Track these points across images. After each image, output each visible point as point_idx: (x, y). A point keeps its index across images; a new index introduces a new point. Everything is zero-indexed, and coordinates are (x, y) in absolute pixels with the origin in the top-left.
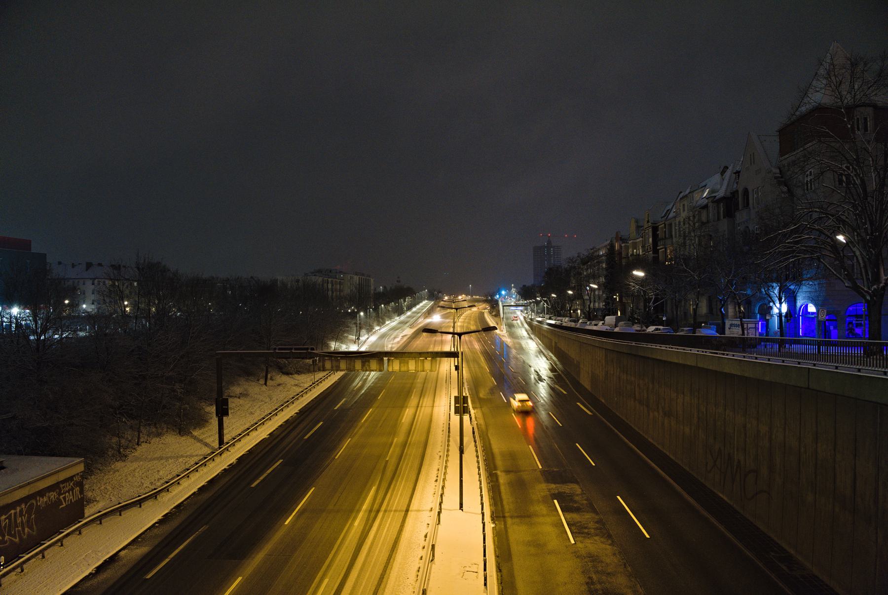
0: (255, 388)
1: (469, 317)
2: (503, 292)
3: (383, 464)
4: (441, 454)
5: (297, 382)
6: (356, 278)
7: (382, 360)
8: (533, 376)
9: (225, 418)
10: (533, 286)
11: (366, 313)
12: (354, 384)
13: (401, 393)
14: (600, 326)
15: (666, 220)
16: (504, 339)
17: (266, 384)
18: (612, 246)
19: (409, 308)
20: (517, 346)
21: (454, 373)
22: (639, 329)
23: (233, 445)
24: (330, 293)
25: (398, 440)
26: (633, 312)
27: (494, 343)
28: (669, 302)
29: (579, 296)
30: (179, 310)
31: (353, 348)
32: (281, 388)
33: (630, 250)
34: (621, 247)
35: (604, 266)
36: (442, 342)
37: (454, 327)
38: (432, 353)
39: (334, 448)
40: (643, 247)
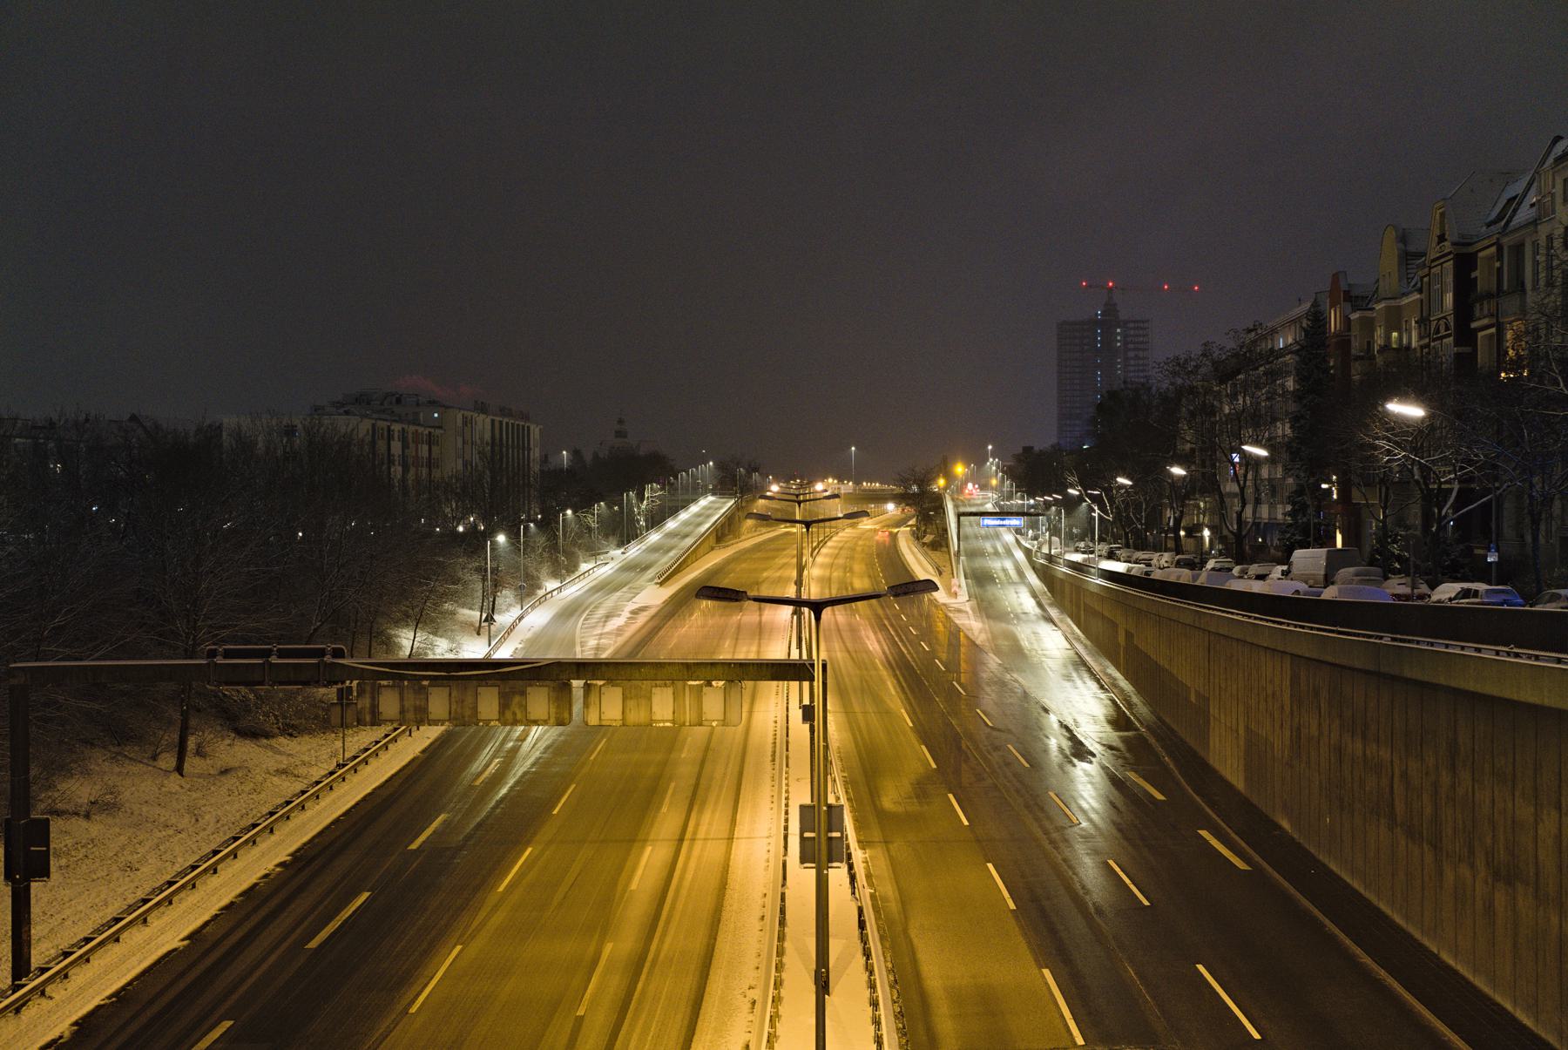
0: (141, 784)
1: (850, 550)
2: (959, 469)
3: (568, 1029)
4: (756, 994)
5: (284, 762)
6: (483, 423)
7: (568, 687)
8: (1055, 743)
9: (35, 886)
10: (1057, 449)
11: (513, 535)
12: (476, 766)
13: (630, 793)
14: (1275, 582)
15: (1504, 232)
16: (960, 621)
17: (179, 769)
18: (1317, 318)
19: (656, 520)
20: (1003, 643)
21: (800, 730)
22: (1406, 590)
23: (64, 975)
24: (397, 471)
25: (617, 948)
26: (1384, 535)
27: (928, 633)
28: (1508, 506)
29: (1205, 483)
30: (705, 463)
31: (474, 649)
32: (230, 781)
33: (1379, 334)
34: (1347, 322)
35: (1290, 384)
36: (761, 632)
37: (799, 583)
38: (727, 665)
39: (405, 977)
40: (1423, 322)
